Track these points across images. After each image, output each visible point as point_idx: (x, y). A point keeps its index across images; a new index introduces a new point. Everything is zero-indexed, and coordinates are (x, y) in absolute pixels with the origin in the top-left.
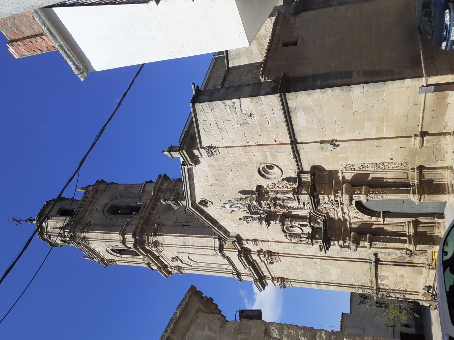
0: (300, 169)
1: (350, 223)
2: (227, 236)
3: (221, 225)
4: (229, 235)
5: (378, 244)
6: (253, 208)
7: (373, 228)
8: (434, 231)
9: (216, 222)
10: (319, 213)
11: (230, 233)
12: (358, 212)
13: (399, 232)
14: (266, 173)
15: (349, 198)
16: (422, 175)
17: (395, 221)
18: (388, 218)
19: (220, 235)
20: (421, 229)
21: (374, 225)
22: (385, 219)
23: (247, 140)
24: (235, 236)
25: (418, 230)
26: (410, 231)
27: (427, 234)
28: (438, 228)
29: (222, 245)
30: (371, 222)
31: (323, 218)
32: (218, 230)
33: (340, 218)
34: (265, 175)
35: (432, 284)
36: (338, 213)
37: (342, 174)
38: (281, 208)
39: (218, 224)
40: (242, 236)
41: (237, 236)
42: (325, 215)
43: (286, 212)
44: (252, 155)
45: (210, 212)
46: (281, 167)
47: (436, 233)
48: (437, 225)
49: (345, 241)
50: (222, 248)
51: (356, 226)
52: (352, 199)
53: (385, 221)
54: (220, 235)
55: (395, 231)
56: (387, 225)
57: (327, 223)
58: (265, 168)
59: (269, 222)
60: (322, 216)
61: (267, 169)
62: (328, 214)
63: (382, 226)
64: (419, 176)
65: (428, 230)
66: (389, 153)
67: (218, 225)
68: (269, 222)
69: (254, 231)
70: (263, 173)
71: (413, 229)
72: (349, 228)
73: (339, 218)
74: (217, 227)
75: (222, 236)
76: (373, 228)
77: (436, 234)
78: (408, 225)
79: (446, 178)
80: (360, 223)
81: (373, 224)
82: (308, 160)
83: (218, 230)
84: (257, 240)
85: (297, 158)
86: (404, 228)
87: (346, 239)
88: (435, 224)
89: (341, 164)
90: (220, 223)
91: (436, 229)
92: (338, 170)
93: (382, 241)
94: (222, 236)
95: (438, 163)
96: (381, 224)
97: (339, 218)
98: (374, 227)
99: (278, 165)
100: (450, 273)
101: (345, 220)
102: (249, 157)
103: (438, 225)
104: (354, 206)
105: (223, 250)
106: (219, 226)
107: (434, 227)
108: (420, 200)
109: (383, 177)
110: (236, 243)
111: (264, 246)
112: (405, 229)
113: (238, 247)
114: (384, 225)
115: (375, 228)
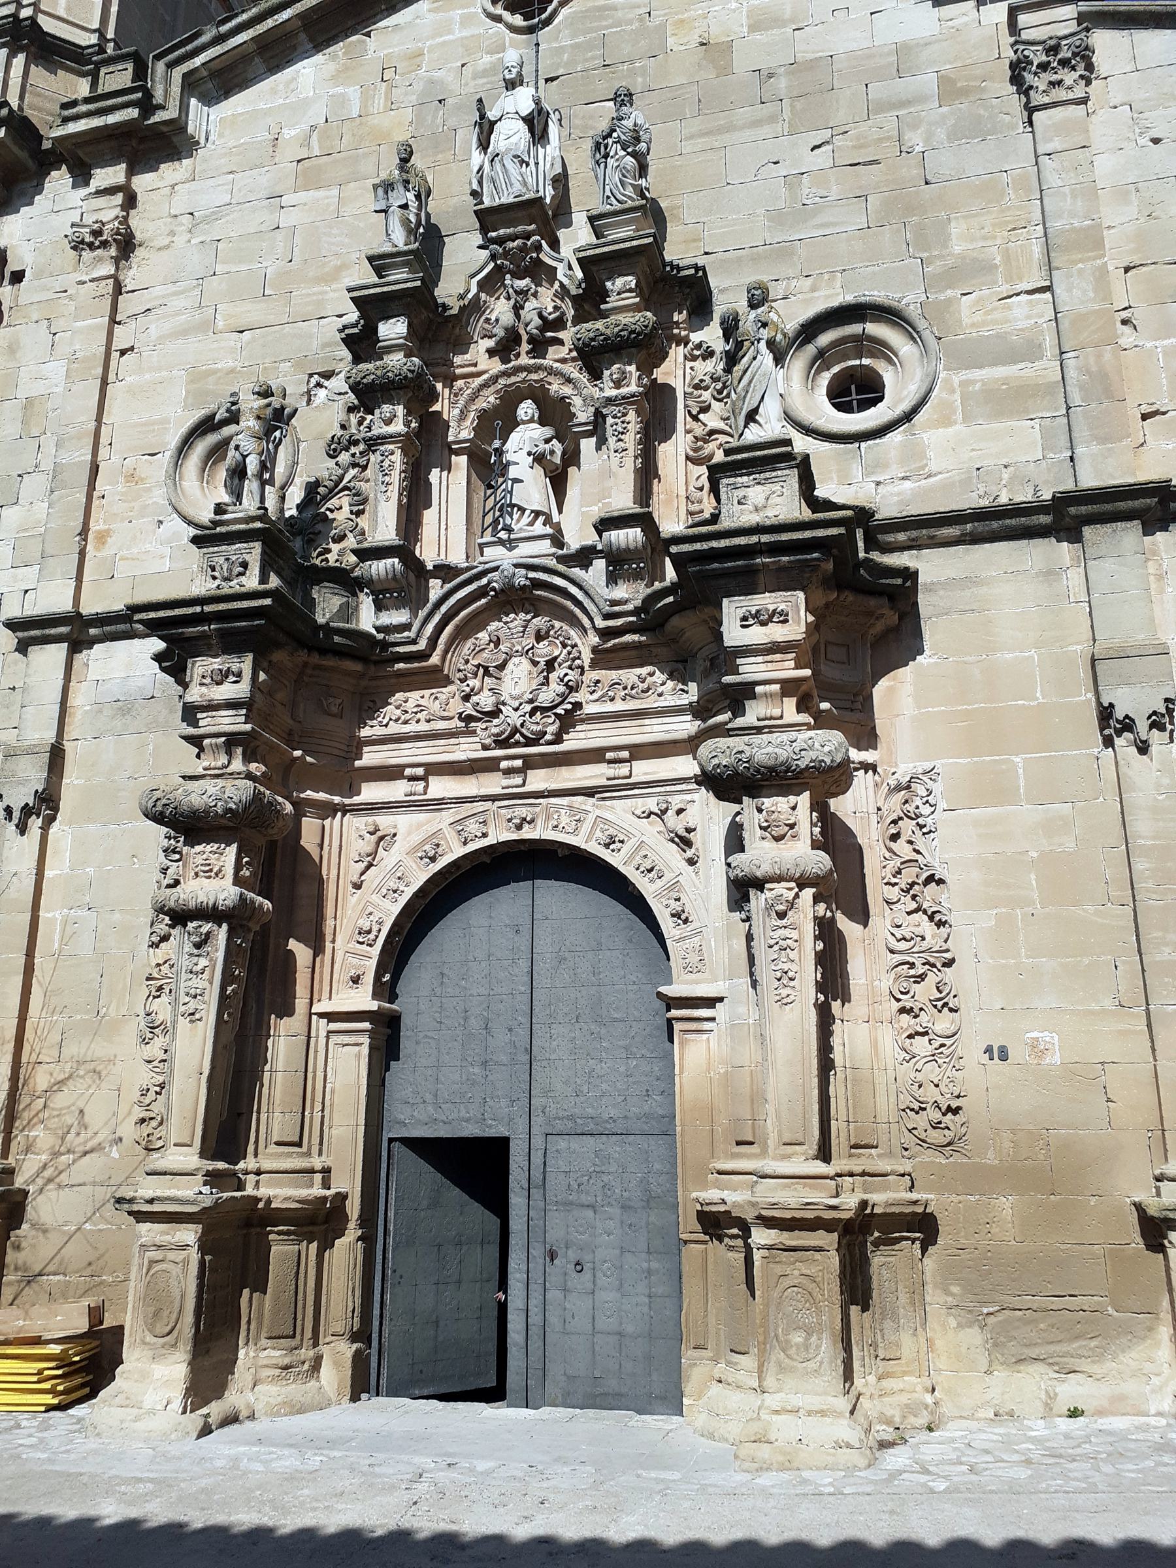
0: (905, 530)
1: (328, 810)
2: (197, 76)
3: (289, 62)
4: (196, 93)
5: (203, 962)
6: (527, 236)
7: (293, 944)
8: (264, 1342)
9: (330, 35)
10: (457, 626)
11: (209, 100)
12: (433, 859)
13: (259, 1112)
14: (821, 353)
15: (802, 764)
16: (897, 1235)
17: (328, 1086)
18: (366, 1040)
19: (224, 29)
20: (281, 1250)
21: (311, 952)
22: (366, 1025)
23: (1144, 269)
24: (187, 123)
25: (279, 1233)
26: (268, 1186)
27: (246, 1292)
28: (286, 1368)
29: (55, 62)
30: (333, 941)
31: (414, 642)
32: (270, 23)
33: (365, 756)
34: (810, 350)
35: (1158, 1345)
36: (431, 743)
37: (860, 763)
38: (483, 415)
39: (311, 40)
40: (169, 172)
41: (175, 139)
42: (435, 659)
43: (451, 439)
44: (1009, 280)
45: (429, 11)
46: (895, 437)
47: (252, 1354)
48: (302, 1357)
49: (239, 750)
50: (33, 49)
51: (308, 841)
52: (764, 791)
53: (334, 1026)
54: (224, 29)
55: (262, 1085)
56: (309, 1037)
57: (357, 667)
58: (846, 358)
59: (401, 311)
60: (433, 641)
61: (836, 369)
62: (436, 678)
63: (301, 1004)
64: (907, 1215)
65: (276, 1300)
66: (1056, 1037)
67: (303, 36)
68: (401, 311)
69: (220, 244)
70: (824, 339)
71: (299, 1202)
72: (302, 795)
73: (366, 749)
74: (288, 28)
75: (204, 39)
76: (293, 944)
77: (247, 1354)
78: (312, 1171)
79: (887, 1384)
80: (329, 872)
81: (317, 945)
82: (969, 581)
83: (270, 23)
84: (127, 258)
85: (1008, 522)
86: (278, 1144)
87: (248, 758)
88: (308, 1342)
89: (939, 764)
90: (319, 58)
91: (278, 1353)
92: (876, 749)
93: (230, 989)
94: (204, 39)
95: (960, 1325)
96: (316, 997)
97: (366, 749)
98: (300, 951)
99: (918, 419)
100: (1020, 1533)
101: (351, 780)
102: (996, 267)
103: (304, 1363)
104: (1150, 721)
105: (21, 49)
106: (294, 48)
107: (293, 1336)
108: (769, 1223)
109: (849, 1001)
110: (133, 113)
111: (51, 296)
112: (273, 1148)
113: (83, 121)
114: (311, 1014)
115: (290, 955)
